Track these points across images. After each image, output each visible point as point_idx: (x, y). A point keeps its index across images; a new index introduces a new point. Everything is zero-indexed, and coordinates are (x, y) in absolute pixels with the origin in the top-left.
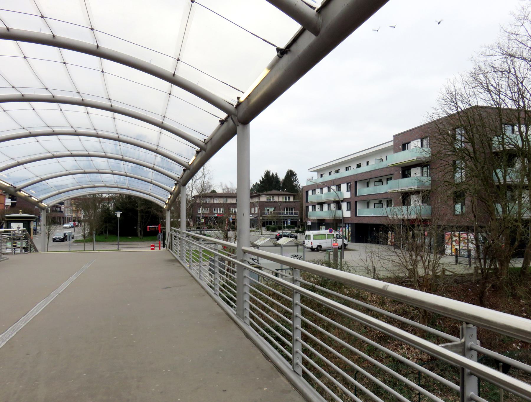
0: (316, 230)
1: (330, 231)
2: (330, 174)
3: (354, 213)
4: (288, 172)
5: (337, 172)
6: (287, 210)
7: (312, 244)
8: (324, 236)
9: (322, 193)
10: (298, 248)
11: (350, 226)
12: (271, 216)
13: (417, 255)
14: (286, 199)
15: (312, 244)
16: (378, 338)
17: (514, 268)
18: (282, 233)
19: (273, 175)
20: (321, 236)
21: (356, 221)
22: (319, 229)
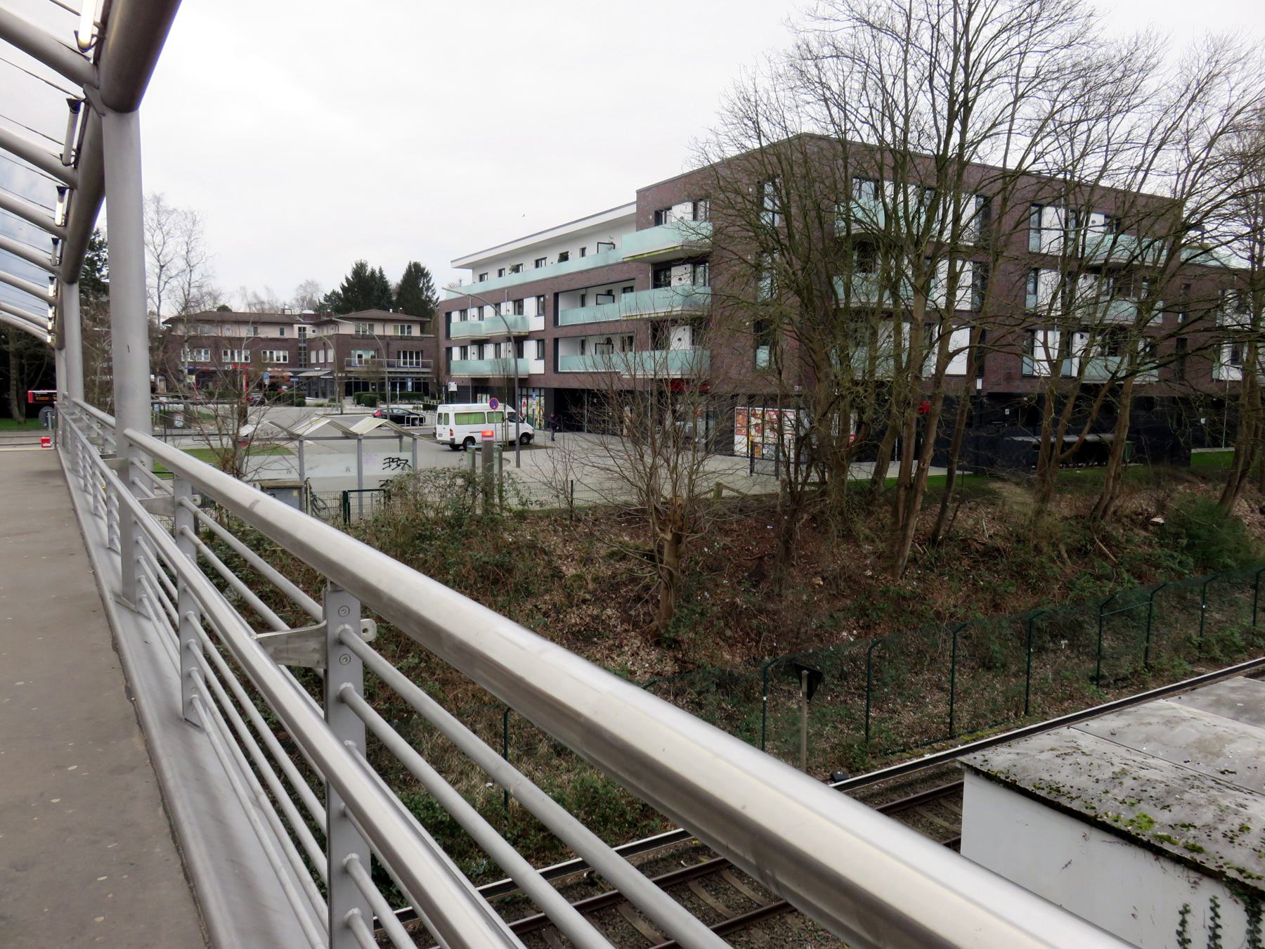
0: (468, 402)
1: (493, 405)
2: (500, 275)
3: (551, 365)
4: (410, 267)
5: (516, 269)
6: (405, 357)
7: (452, 435)
8: (480, 417)
9: (481, 317)
10: (401, 441)
11: (543, 393)
12: (365, 369)
13: (656, 454)
14: (402, 332)
15: (452, 435)
16: (573, 634)
17: (857, 482)
18: (388, 409)
19: (373, 273)
20: (474, 416)
21: (556, 384)
22: (475, 401)
